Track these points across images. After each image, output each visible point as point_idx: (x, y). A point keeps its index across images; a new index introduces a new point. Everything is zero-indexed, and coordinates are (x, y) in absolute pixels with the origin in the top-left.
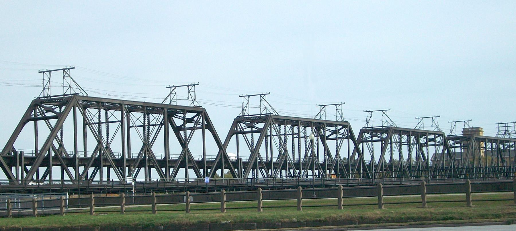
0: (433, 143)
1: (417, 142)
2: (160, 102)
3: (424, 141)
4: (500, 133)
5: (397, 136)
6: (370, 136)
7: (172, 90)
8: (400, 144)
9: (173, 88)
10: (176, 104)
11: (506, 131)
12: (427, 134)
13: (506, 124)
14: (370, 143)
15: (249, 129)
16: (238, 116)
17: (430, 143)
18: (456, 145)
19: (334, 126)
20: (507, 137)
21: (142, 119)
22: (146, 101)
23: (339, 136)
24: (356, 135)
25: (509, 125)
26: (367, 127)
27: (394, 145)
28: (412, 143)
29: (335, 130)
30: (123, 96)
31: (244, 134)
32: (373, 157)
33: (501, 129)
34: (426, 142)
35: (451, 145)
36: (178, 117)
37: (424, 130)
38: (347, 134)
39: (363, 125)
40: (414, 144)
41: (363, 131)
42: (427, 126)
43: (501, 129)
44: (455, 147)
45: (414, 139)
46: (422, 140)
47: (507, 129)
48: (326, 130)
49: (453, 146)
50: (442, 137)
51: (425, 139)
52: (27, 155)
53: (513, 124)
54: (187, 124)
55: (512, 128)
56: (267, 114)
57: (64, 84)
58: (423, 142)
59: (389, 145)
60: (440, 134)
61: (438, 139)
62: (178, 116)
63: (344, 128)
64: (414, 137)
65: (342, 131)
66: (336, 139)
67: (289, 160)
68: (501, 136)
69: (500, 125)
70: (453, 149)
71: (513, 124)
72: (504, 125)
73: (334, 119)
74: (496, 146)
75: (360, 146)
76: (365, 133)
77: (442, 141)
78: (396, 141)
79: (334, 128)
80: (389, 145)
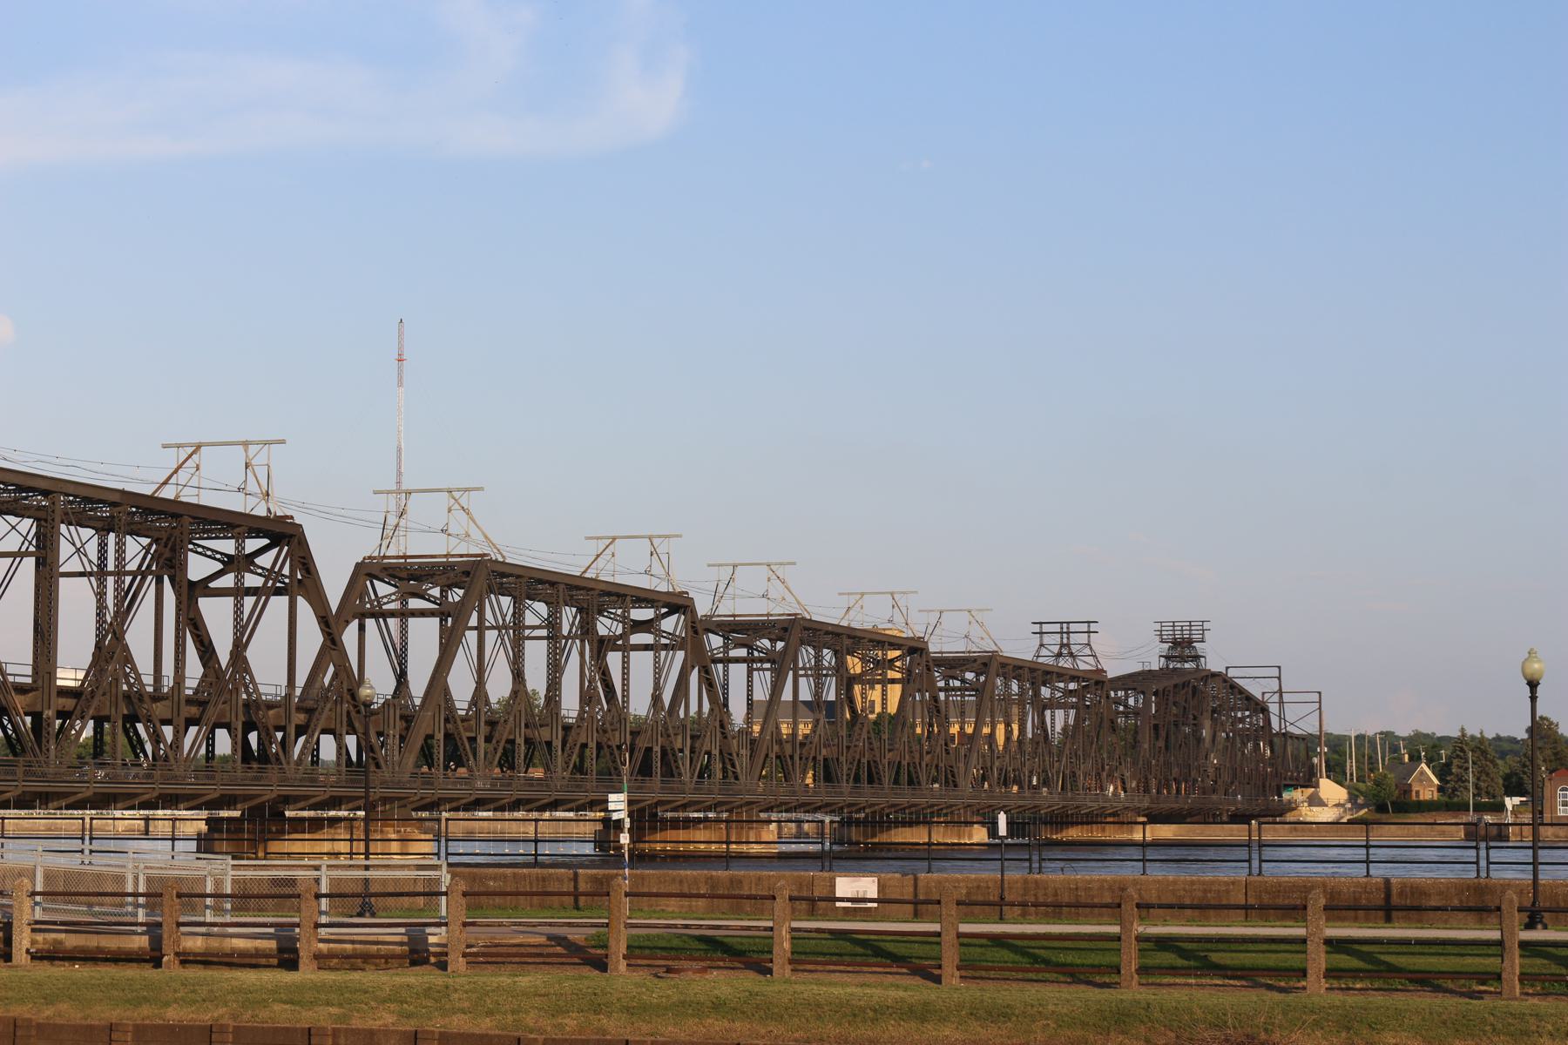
0: (646, 638)
1: (840, 667)
2: (147, 490)
3: (613, 630)
4: (1044, 652)
5: (506, 601)
6: (394, 594)
7: (851, 597)
8: (517, 634)
9: (190, 450)
10: (196, 503)
11: (1062, 645)
12: (887, 644)
13: (1065, 625)
14: (393, 623)
15: (742, 652)
16: (364, 558)
17: (638, 638)
18: (734, 653)
19: (225, 538)
20: (1065, 663)
21: (92, 550)
22: (126, 489)
23: (252, 580)
24: (334, 589)
25: (1073, 627)
26: (385, 557)
27: (491, 636)
28: (565, 632)
29: (232, 551)
30: (515, 556)
31: (381, 620)
32: (402, 677)
33: (1047, 639)
34: (619, 631)
35: (715, 652)
36: (200, 550)
37: (616, 582)
38: (286, 571)
39: (366, 546)
40: (574, 638)
41: (366, 571)
42: (627, 570)
43: (1047, 639)
44: (727, 661)
45: (575, 618)
46: (854, 665)
47: (1065, 641)
48: (191, 550)
49: (721, 655)
50: (683, 617)
51: (615, 623)
52: (16, 681)
53: (1084, 627)
54: (631, 636)
55: (1083, 638)
56: (472, 556)
57: (245, 485)
58: (610, 631)
59: (472, 637)
60: (678, 604)
61: (668, 624)
62: (199, 546)
63: (276, 550)
64: (574, 610)
65: (265, 560)
66: (239, 592)
67: (247, 692)
68: (1046, 660)
69: (1046, 628)
70: (720, 666)
71: (1084, 627)
72: (1057, 628)
73: (235, 503)
74: (831, 658)
75: (350, 636)
76: (710, 634)
77: (683, 635)
78: (504, 620)
79: (227, 546)
80: (472, 637)
